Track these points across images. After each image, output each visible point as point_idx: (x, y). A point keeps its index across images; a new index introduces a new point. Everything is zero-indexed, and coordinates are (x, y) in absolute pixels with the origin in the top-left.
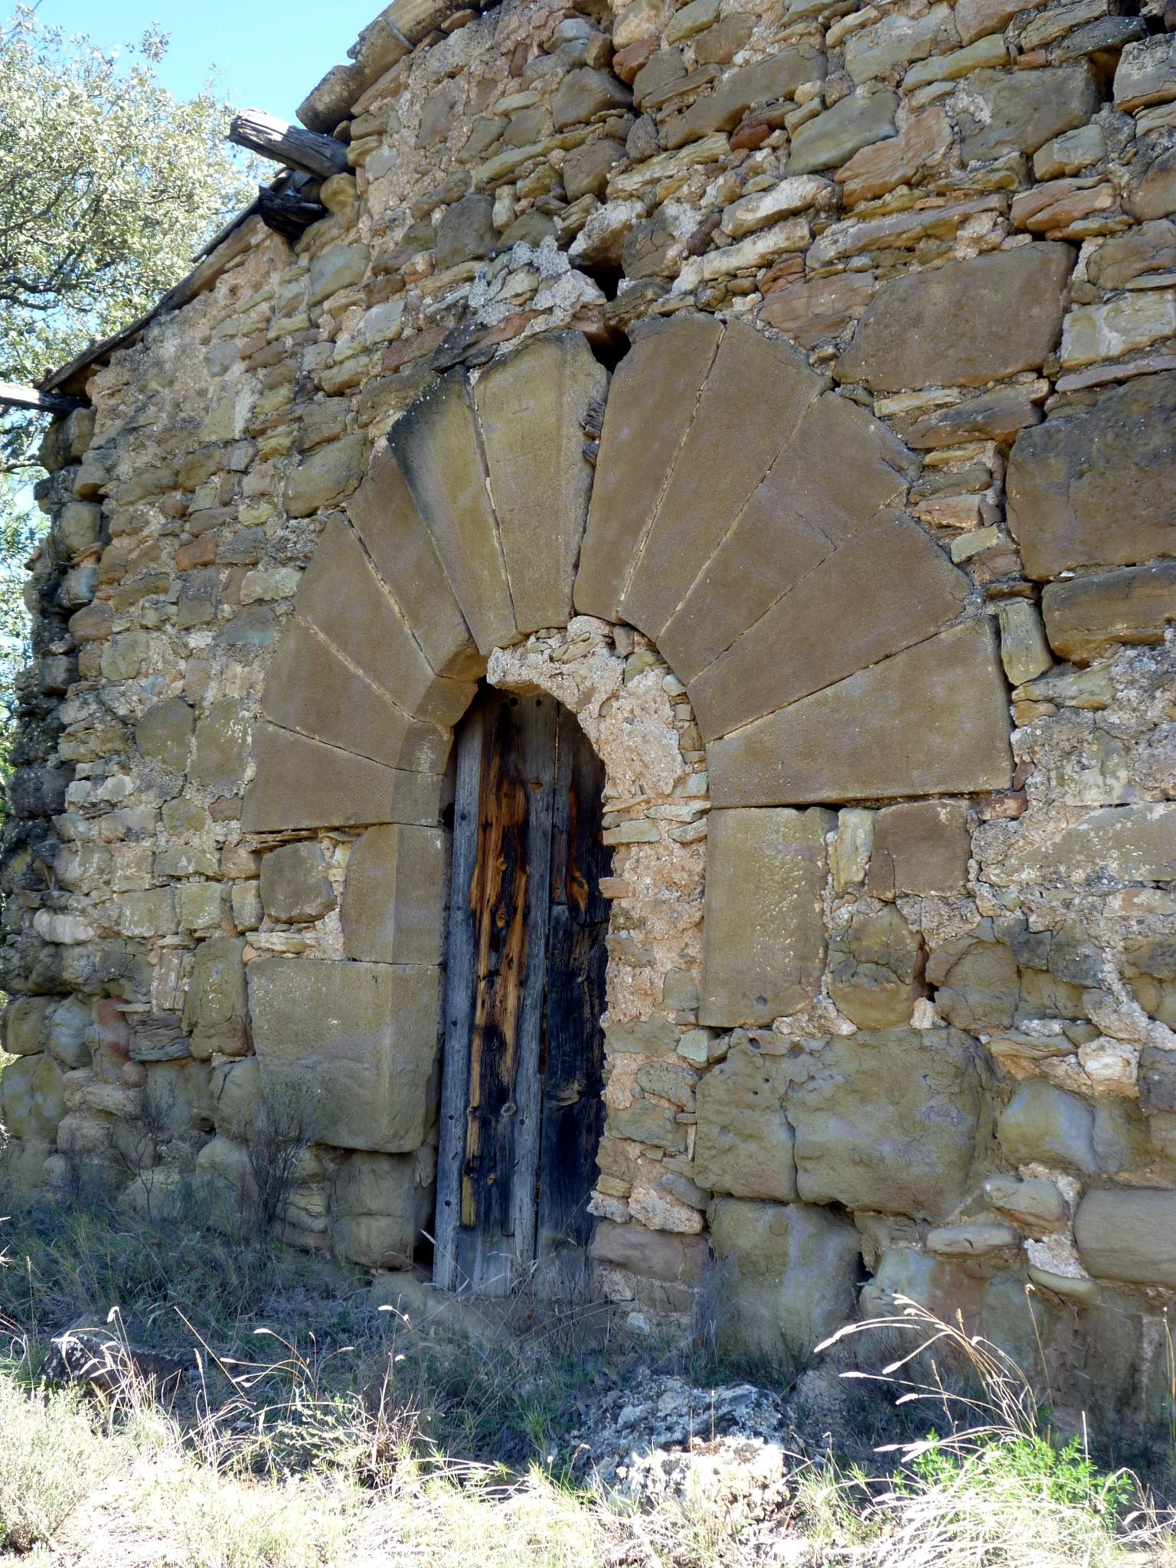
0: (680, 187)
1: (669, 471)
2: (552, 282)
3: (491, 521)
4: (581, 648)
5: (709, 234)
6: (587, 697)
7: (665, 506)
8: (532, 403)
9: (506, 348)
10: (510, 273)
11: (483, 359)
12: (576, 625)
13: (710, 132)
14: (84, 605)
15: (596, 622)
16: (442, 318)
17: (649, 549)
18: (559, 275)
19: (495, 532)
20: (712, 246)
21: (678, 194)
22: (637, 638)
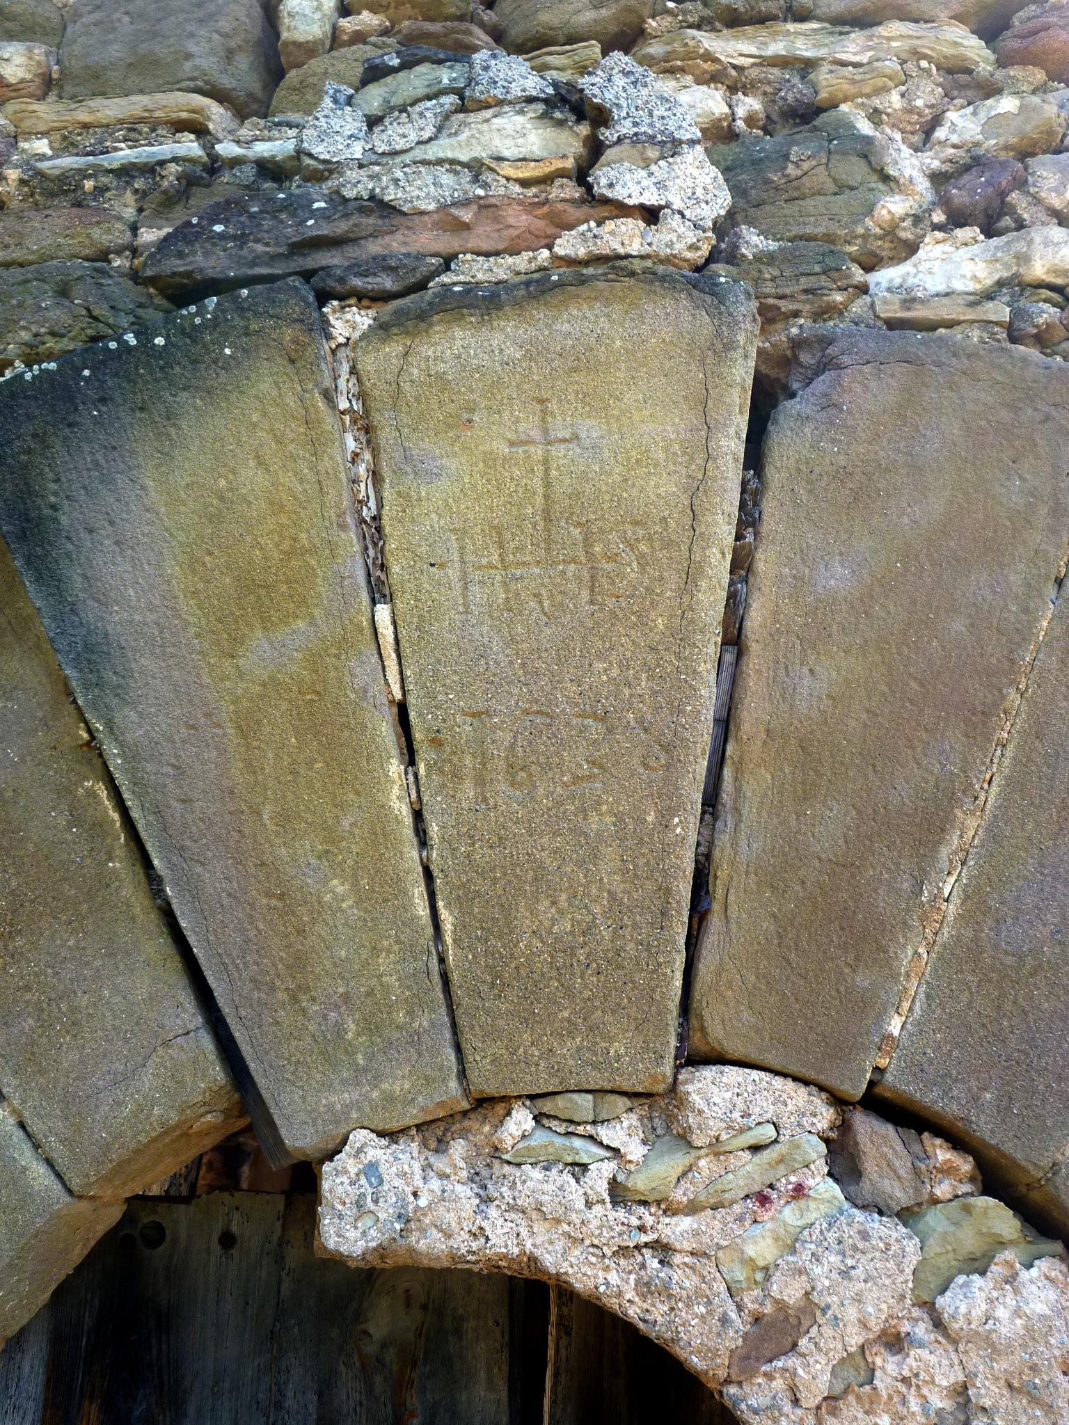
0: (885, 90)
1: (1013, 697)
2: (652, 153)
3: (386, 730)
4: (747, 1171)
5: (1003, 194)
6: (777, 1333)
7: (1011, 783)
8: (591, 429)
9: (478, 270)
10: (462, 109)
11: (387, 283)
12: (715, 1093)
13: (943, 16)
14: (852, 188)
15: (799, 1096)
16: (100, 191)
17: (972, 896)
18: (677, 143)
19: (395, 768)
20: (1007, 221)
21: (876, 102)
22: (942, 1154)
